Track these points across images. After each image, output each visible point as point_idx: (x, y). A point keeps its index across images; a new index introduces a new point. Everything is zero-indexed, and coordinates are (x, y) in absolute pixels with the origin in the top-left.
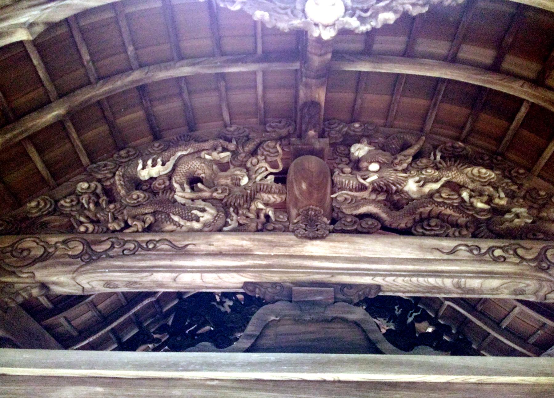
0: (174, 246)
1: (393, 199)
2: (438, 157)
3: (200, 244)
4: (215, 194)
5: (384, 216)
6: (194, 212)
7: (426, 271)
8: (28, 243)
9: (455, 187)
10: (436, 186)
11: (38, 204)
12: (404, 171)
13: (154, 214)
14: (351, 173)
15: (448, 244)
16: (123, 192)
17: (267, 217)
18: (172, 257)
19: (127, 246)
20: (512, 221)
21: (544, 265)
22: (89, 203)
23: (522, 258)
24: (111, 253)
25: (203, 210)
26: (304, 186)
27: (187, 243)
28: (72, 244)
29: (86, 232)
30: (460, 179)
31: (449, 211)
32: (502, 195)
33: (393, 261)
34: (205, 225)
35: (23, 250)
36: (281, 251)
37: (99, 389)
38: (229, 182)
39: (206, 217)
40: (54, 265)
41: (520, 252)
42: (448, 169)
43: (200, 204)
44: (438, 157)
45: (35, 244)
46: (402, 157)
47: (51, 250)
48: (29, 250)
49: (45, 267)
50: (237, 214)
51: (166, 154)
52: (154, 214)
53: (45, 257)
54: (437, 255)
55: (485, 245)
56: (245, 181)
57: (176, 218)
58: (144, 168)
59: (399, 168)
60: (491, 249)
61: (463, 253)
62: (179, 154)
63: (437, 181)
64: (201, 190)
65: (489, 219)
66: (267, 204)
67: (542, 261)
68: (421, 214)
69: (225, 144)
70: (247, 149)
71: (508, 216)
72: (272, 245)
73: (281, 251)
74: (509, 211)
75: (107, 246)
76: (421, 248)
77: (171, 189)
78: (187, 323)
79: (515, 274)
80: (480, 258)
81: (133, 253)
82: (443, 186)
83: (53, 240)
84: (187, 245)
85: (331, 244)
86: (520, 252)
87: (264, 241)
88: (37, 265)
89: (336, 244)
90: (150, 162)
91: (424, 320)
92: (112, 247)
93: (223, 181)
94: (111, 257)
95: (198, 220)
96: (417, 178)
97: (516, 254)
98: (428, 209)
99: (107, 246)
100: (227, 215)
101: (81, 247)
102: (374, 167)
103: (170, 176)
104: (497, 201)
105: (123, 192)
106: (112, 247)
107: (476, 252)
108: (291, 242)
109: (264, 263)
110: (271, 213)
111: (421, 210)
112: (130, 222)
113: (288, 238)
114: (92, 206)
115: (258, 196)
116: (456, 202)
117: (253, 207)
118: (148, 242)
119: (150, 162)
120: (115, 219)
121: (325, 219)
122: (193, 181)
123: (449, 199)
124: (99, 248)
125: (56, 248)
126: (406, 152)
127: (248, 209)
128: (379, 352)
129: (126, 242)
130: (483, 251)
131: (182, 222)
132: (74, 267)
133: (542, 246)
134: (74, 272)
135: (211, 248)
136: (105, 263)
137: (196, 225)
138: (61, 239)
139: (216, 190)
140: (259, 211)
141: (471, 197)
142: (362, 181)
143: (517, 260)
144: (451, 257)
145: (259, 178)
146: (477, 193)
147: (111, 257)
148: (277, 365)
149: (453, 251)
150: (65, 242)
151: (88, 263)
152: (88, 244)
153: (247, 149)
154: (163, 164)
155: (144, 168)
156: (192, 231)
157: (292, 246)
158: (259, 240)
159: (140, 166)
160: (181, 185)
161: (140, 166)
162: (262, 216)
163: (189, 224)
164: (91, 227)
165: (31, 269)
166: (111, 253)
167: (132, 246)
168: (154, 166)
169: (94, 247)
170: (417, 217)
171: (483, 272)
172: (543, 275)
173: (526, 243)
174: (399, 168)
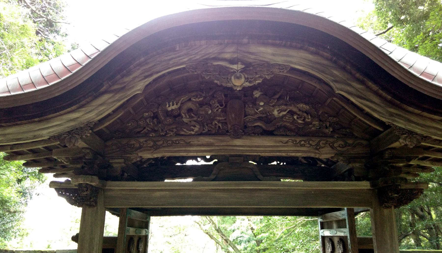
0: (186, 143)
1: (268, 119)
2: (288, 98)
3: (195, 141)
4: (199, 119)
5: (264, 127)
6: (192, 127)
7: (277, 150)
8: (133, 142)
9: (292, 113)
10: (284, 113)
11: (131, 124)
12: (273, 106)
13: (176, 128)
14: (252, 107)
15: (285, 139)
16: (163, 118)
17: (219, 127)
18: (185, 146)
19: (168, 142)
20: (311, 128)
21: (318, 147)
22: (150, 122)
23: (311, 145)
24: (164, 145)
25: (195, 126)
26: (233, 116)
27: (190, 141)
28: (149, 142)
29: (152, 137)
30: (295, 110)
31: (288, 124)
32: (310, 117)
33: (265, 147)
34: (196, 132)
35: (131, 145)
36: (224, 144)
37: (167, 193)
38: (204, 113)
39: (196, 129)
40: (144, 150)
41: (311, 142)
42: (290, 105)
43: (194, 123)
44: (288, 98)
45: (135, 142)
46: (273, 100)
47: (142, 144)
48: (134, 144)
49: (141, 151)
50: (208, 126)
51: (177, 99)
52: (176, 128)
53: (140, 147)
54: (281, 144)
55: (298, 140)
56: (210, 112)
57: (185, 130)
58: (169, 106)
59: (271, 105)
60: (301, 141)
61: (290, 144)
62: (182, 99)
63: (285, 111)
64: (193, 117)
65: (303, 127)
66: (219, 122)
67: (318, 146)
68: (278, 125)
69: (201, 93)
70: (210, 94)
71: (310, 126)
72: (222, 141)
73: (224, 144)
74: (311, 124)
75: (161, 142)
76: (276, 142)
77: (180, 115)
78: (178, 164)
79: (307, 151)
80: (296, 145)
81: (171, 145)
82: (288, 112)
83: (142, 140)
84: (190, 142)
85: (243, 140)
86: (311, 142)
87: (218, 139)
88: (138, 150)
89: (245, 140)
90: (171, 103)
91: (118, 215)
92: (163, 143)
93: (201, 113)
94: (164, 147)
95: (193, 131)
96: (278, 109)
97: (309, 143)
98: (280, 124)
99: (161, 142)
100: (204, 126)
101: (152, 143)
102: (262, 104)
103: (180, 108)
104: (307, 120)
105: (163, 118)
106: (163, 143)
107: (295, 143)
108: (228, 140)
109: (219, 148)
110: (220, 126)
111: (278, 124)
112: (168, 132)
113: (227, 138)
114: (151, 123)
115: (215, 118)
116: (291, 121)
117: (213, 123)
118: (176, 141)
119: (171, 103)
120: (162, 130)
121: (241, 131)
122: (190, 110)
123: (288, 120)
124: (159, 143)
125: (144, 144)
126: (274, 97)
127: (212, 123)
128: (260, 180)
129: (168, 141)
130: (297, 142)
131: (187, 131)
132: (152, 151)
133: (319, 140)
134: (152, 153)
135: (200, 143)
136: (162, 149)
137: (193, 133)
138: (144, 140)
139: (199, 117)
140: (216, 124)
141: (297, 118)
142: (256, 111)
143: (309, 146)
144: (286, 145)
145: (215, 110)
146: (299, 117)
147: (164, 147)
148: (224, 185)
149: (287, 142)
150: (146, 141)
151: (156, 149)
152: (154, 142)
153: (210, 94)
154: (177, 104)
155: (169, 106)
156: (191, 135)
157: (229, 141)
158: (216, 139)
159: (168, 106)
160: (185, 114)
161: (168, 106)
162: (217, 127)
163: (190, 132)
164: (154, 134)
165: (136, 152)
166: (164, 145)
167: (170, 142)
168: (173, 105)
169: (157, 143)
170: (276, 127)
171: (296, 151)
172: (317, 151)
173: (314, 139)
174: (271, 105)
